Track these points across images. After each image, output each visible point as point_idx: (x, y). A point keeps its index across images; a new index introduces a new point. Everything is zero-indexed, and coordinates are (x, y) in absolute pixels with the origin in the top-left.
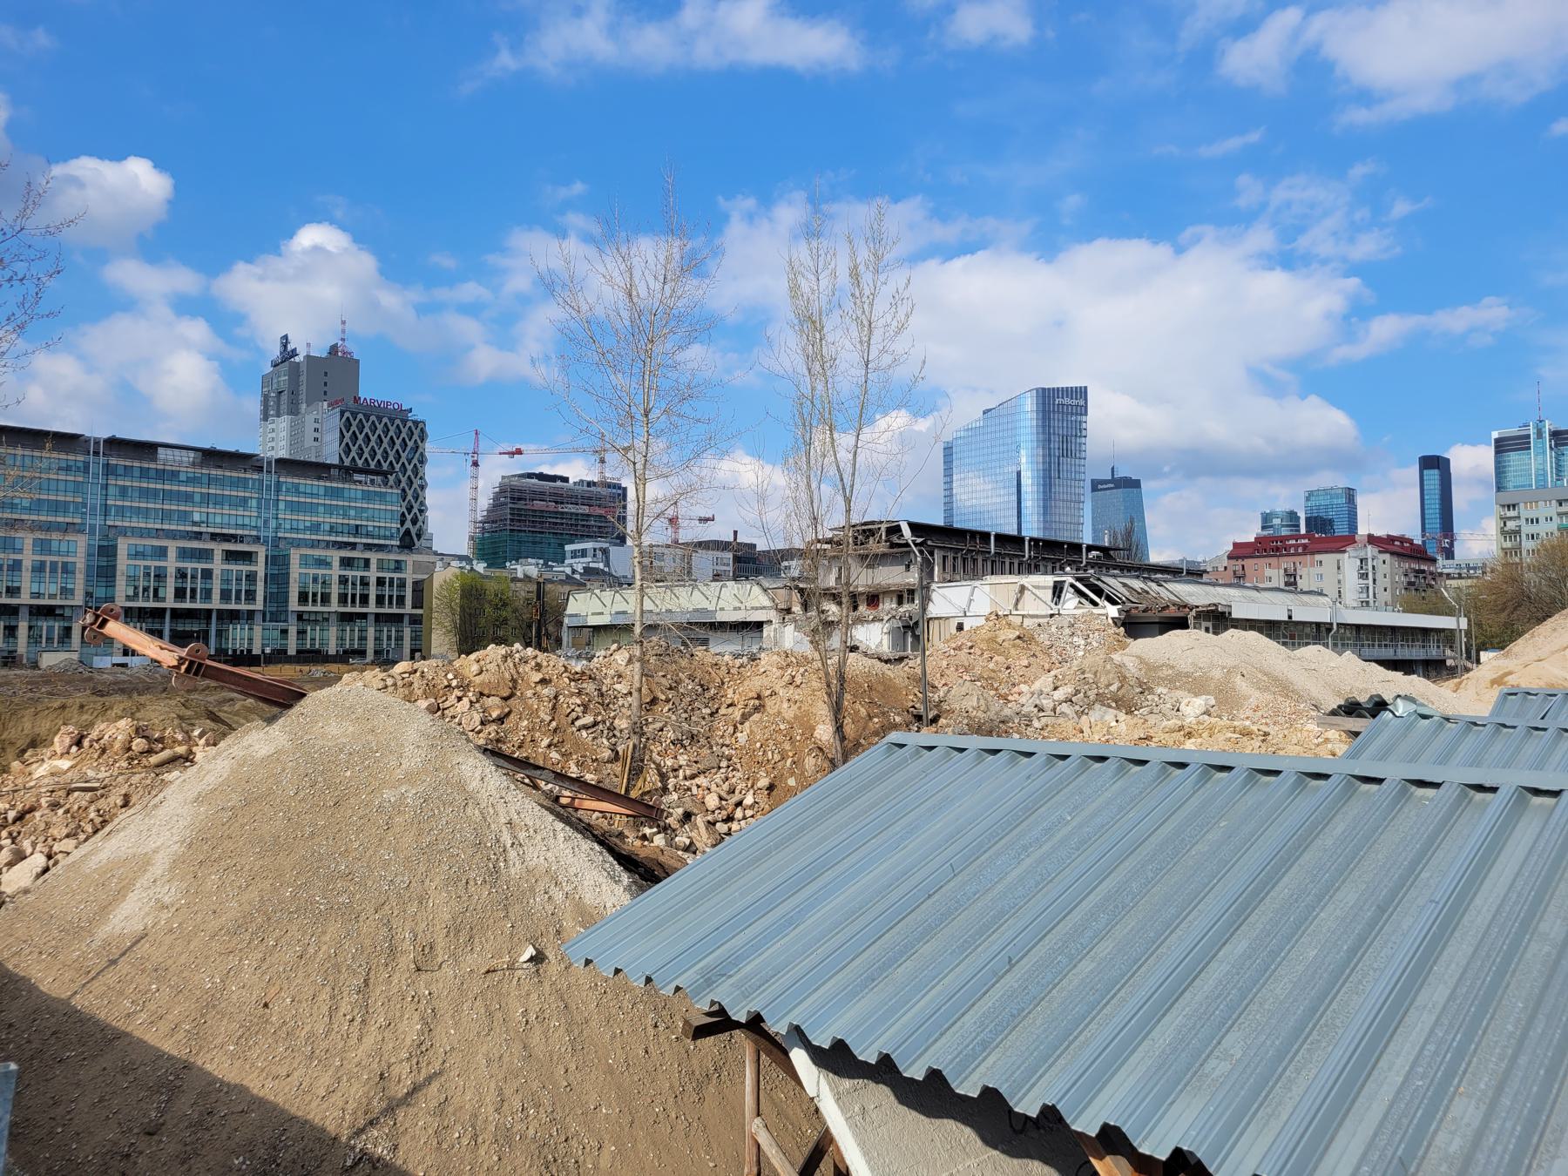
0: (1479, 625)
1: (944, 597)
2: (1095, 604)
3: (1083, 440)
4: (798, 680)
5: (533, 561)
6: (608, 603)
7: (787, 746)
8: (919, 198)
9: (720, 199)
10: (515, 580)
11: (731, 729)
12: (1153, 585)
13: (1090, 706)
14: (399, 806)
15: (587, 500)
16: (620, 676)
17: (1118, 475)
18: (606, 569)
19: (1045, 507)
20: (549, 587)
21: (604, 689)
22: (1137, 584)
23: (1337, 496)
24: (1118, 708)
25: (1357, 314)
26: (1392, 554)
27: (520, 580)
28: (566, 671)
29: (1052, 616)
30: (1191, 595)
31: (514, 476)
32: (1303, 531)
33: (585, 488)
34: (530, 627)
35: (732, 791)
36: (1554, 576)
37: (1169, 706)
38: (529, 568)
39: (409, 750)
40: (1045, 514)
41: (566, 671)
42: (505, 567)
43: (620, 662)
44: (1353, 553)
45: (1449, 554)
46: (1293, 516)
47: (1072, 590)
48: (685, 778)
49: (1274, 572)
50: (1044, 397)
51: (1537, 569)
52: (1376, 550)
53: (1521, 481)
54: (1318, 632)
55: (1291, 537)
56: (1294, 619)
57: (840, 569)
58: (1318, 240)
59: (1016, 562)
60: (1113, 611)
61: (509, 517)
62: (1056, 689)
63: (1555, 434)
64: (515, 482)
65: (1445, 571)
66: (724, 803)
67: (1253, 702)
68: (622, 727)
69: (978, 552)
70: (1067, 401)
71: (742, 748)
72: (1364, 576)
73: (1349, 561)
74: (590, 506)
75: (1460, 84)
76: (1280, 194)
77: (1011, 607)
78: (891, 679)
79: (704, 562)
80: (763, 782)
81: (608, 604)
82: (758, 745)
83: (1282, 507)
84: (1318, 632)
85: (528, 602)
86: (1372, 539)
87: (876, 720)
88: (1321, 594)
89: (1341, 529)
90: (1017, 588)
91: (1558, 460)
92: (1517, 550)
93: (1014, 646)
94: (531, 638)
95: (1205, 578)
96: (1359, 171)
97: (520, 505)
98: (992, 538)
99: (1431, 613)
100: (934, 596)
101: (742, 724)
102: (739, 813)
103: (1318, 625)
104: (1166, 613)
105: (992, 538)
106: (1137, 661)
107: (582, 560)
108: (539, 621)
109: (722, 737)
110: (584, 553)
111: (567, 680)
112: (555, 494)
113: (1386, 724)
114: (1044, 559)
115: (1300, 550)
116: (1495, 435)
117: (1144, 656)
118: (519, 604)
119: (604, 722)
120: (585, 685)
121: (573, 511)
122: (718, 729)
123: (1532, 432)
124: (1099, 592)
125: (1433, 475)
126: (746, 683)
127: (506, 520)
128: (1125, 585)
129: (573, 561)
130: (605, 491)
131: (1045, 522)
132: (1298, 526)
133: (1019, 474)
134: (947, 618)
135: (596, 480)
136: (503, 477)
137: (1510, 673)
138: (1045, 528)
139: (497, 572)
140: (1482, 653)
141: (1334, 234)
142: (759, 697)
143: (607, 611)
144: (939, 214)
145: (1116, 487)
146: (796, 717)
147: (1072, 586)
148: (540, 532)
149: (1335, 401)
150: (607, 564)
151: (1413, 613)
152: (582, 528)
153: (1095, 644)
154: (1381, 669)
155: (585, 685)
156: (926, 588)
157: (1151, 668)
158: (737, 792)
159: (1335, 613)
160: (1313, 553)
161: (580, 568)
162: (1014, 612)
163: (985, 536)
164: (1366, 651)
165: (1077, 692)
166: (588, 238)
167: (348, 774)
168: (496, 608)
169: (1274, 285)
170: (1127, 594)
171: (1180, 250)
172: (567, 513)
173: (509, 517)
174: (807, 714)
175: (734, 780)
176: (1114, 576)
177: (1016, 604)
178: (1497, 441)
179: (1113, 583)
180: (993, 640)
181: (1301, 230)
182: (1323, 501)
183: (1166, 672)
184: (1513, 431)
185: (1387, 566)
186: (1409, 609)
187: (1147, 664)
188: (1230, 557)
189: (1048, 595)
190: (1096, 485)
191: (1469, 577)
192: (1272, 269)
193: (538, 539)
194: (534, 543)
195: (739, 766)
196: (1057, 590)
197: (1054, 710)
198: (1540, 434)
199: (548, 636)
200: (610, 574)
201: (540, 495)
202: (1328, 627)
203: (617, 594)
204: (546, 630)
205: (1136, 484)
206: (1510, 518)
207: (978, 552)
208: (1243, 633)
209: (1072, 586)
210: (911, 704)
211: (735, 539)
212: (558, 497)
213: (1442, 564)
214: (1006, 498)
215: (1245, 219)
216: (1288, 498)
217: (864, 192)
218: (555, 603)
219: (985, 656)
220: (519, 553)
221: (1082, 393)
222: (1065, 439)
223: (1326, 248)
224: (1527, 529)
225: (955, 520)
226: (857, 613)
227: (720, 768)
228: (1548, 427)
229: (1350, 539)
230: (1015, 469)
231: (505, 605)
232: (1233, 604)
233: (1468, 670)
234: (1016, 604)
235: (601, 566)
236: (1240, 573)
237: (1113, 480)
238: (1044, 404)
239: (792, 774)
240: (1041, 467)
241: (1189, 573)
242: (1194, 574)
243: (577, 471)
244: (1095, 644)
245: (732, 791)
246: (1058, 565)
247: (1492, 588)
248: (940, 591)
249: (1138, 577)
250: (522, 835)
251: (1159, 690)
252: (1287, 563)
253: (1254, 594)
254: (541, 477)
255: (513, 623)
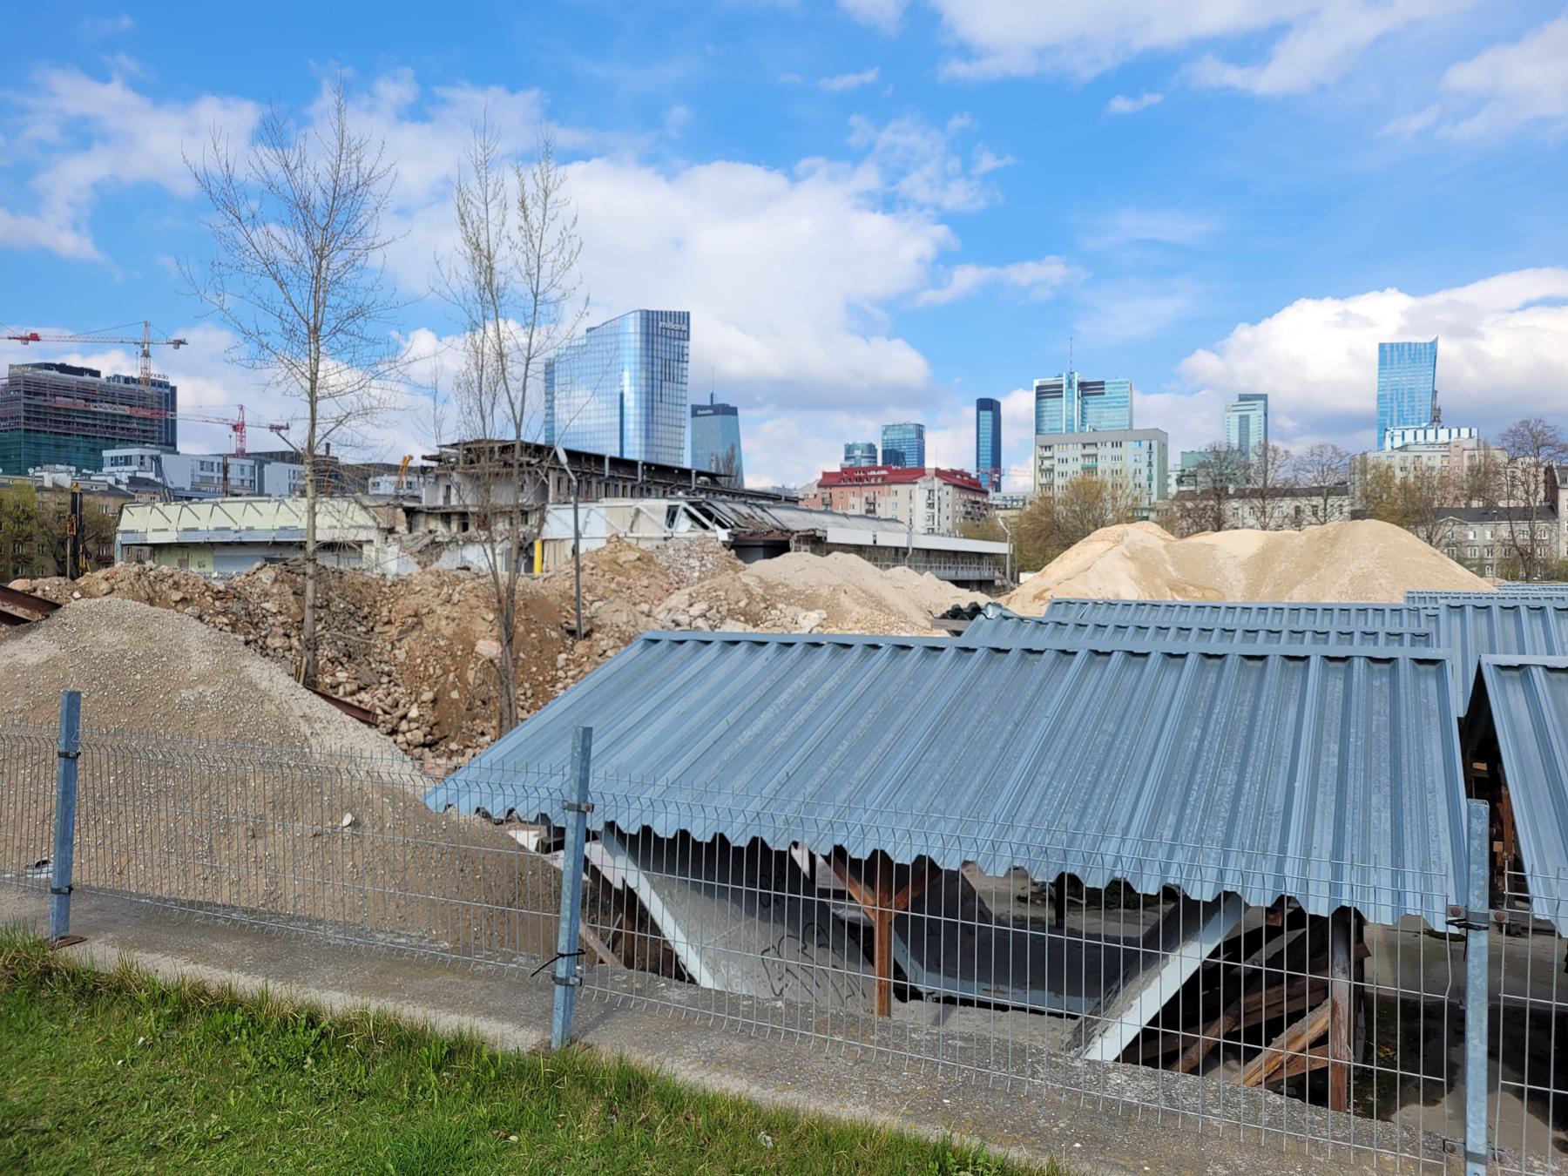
0: (1021, 551)
1: (559, 518)
2: (705, 527)
3: (685, 365)
4: (456, 598)
5: (63, 468)
6: (174, 518)
7: (448, 661)
8: (534, 94)
9: (312, 63)
10: (41, 489)
11: (389, 647)
12: (759, 511)
13: (722, 620)
14: (200, 704)
15: (128, 399)
16: (266, 595)
17: (717, 401)
18: (159, 480)
19: (647, 431)
20: (86, 498)
21: (251, 607)
22: (744, 510)
23: (910, 432)
24: (746, 622)
25: (945, 260)
26: (955, 486)
27: (47, 490)
28: (208, 589)
29: (665, 539)
30: (791, 520)
31: (27, 366)
32: (880, 463)
33: (122, 384)
34: (63, 544)
35: (396, 705)
36: (1077, 509)
37: (789, 619)
38: (59, 476)
39: (194, 654)
40: (647, 437)
41: (208, 589)
42: (26, 473)
43: (264, 580)
44: (923, 485)
45: (997, 486)
46: (871, 448)
47: (685, 514)
48: (345, 694)
49: (855, 501)
50: (648, 319)
51: (1064, 502)
52: (942, 482)
53: (1054, 425)
54: (897, 555)
55: (870, 469)
56: (878, 543)
57: (448, 488)
58: (915, 185)
59: (629, 485)
60: (723, 535)
61: (23, 414)
62: (691, 605)
63: (1082, 385)
64: (29, 373)
65: (995, 502)
66: (388, 717)
67: (854, 615)
68: (277, 645)
69: (592, 474)
70: (670, 325)
71: (402, 664)
72: (931, 506)
73: (919, 491)
74: (131, 406)
75: (1041, 53)
76: (886, 137)
77: (627, 530)
78: (544, 597)
79: (276, 474)
80: (428, 696)
81: (174, 520)
82: (419, 661)
83: (862, 439)
84: (897, 555)
85: (59, 516)
86: (939, 473)
87: (533, 635)
88: (896, 521)
89: (911, 463)
90: (633, 512)
91: (1083, 408)
92: (1050, 485)
93: (634, 567)
94: (64, 557)
95: (802, 505)
96: (958, 122)
97: (38, 401)
98: (607, 461)
99: (984, 539)
100: (549, 518)
101: (399, 640)
102: (404, 726)
103: (897, 549)
104: (770, 538)
105: (607, 461)
106: (757, 581)
107: (126, 468)
108: (75, 538)
109: (380, 654)
110: (127, 461)
111: (209, 599)
112: (85, 391)
113: (981, 624)
114: (656, 483)
115: (879, 481)
116: (1037, 383)
117: (763, 576)
118: (49, 517)
119: (256, 641)
120: (230, 604)
121: (109, 411)
122: (375, 646)
123: (1065, 382)
124: (710, 516)
125: (987, 416)
126: (400, 601)
127: (19, 417)
128: (733, 510)
129: (114, 469)
130: (149, 390)
131: (647, 445)
132: (875, 458)
133: (622, 396)
134: (563, 540)
135: (136, 376)
136: (11, 367)
137: (1048, 590)
138: (646, 452)
139: (18, 480)
140: (1021, 575)
141: (929, 181)
142: (416, 615)
143: (172, 527)
144: (553, 113)
145: (716, 413)
146: (455, 633)
147: (686, 510)
148: (65, 434)
149: (916, 343)
150: (159, 472)
151: (984, 539)
152: (120, 432)
153: (709, 566)
154: (953, 586)
155: (230, 604)
156: (542, 509)
157: (769, 587)
158: (400, 706)
159: (910, 540)
160: (890, 484)
161: (124, 478)
162: (630, 535)
163: (599, 459)
164: (942, 573)
165: (711, 608)
166: (134, 85)
167: (138, 677)
168: (18, 521)
169: (875, 227)
170: (735, 518)
171: (794, 179)
172: (100, 413)
173: (23, 414)
174: (466, 630)
175: (396, 695)
176: (724, 501)
177: (632, 526)
178: (1038, 388)
179: (723, 508)
180: (615, 561)
181: (902, 174)
182: (894, 435)
183: (781, 590)
184: (1050, 381)
185: (949, 497)
186: (967, 536)
187: (765, 583)
188: (819, 486)
189: (663, 519)
190: (696, 411)
191: (1012, 508)
192: (874, 211)
193: (62, 442)
194: (58, 446)
195: (400, 681)
196: (672, 515)
197: (690, 624)
198: (1070, 384)
199: (87, 554)
200: (165, 486)
201: (66, 391)
202: (905, 551)
203: (185, 509)
204: (84, 547)
205: (733, 411)
206: (1047, 458)
207: (592, 474)
208: (845, 555)
209: (686, 510)
210: (564, 620)
211: (328, 452)
212: (89, 395)
213: (993, 497)
214: (609, 420)
215: (856, 158)
216: (869, 431)
217: (481, 80)
218: (95, 518)
219: (607, 577)
220: (38, 457)
221: (685, 317)
222: (667, 363)
223: (922, 194)
224: (1059, 468)
225: (556, 439)
226: (466, 534)
227: (381, 684)
228: (1076, 379)
229: (920, 472)
230: (618, 390)
231: (29, 518)
232: (829, 530)
233: (1012, 589)
234: (632, 526)
235: (152, 476)
236: (827, 501)
237: (712, 407)
238: (648, 326)
239: (455, 687)
240: (644, 390)
241: (787, 500)
242: (792, 501)
243: (112, 364)
244: (709, 566)
245: (396, 705)
246: (668, 489)
247: (1030, 517)
248: (555, 512)
249: (745, 503)
250: (318, 726)
251: (780, 606)
252: (867, 492)
253: (844, 520)
254: (63, 368)
255: (39, 539)
